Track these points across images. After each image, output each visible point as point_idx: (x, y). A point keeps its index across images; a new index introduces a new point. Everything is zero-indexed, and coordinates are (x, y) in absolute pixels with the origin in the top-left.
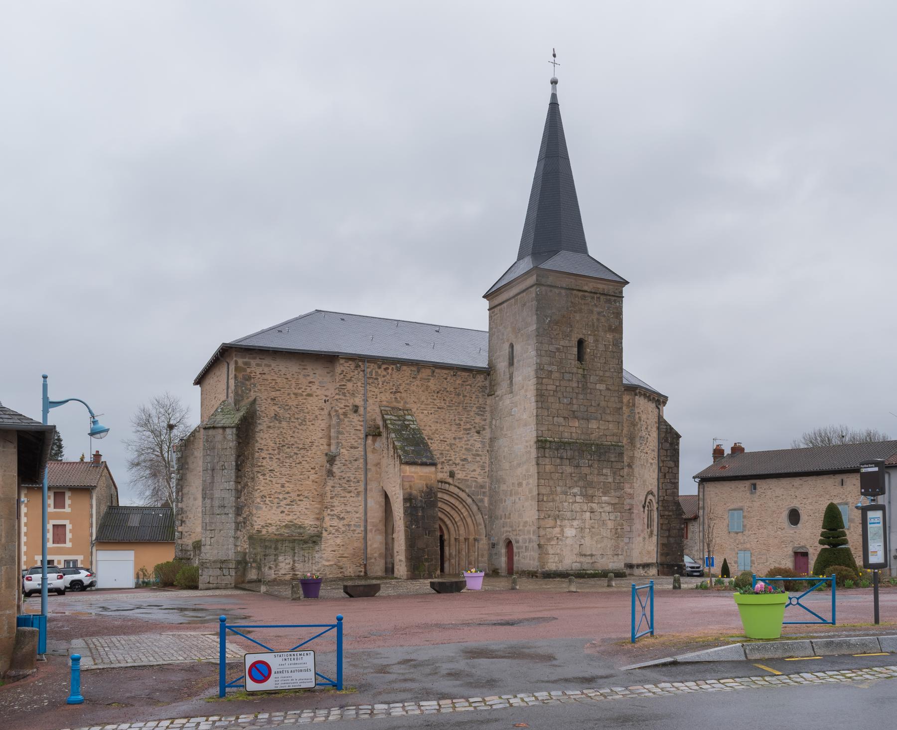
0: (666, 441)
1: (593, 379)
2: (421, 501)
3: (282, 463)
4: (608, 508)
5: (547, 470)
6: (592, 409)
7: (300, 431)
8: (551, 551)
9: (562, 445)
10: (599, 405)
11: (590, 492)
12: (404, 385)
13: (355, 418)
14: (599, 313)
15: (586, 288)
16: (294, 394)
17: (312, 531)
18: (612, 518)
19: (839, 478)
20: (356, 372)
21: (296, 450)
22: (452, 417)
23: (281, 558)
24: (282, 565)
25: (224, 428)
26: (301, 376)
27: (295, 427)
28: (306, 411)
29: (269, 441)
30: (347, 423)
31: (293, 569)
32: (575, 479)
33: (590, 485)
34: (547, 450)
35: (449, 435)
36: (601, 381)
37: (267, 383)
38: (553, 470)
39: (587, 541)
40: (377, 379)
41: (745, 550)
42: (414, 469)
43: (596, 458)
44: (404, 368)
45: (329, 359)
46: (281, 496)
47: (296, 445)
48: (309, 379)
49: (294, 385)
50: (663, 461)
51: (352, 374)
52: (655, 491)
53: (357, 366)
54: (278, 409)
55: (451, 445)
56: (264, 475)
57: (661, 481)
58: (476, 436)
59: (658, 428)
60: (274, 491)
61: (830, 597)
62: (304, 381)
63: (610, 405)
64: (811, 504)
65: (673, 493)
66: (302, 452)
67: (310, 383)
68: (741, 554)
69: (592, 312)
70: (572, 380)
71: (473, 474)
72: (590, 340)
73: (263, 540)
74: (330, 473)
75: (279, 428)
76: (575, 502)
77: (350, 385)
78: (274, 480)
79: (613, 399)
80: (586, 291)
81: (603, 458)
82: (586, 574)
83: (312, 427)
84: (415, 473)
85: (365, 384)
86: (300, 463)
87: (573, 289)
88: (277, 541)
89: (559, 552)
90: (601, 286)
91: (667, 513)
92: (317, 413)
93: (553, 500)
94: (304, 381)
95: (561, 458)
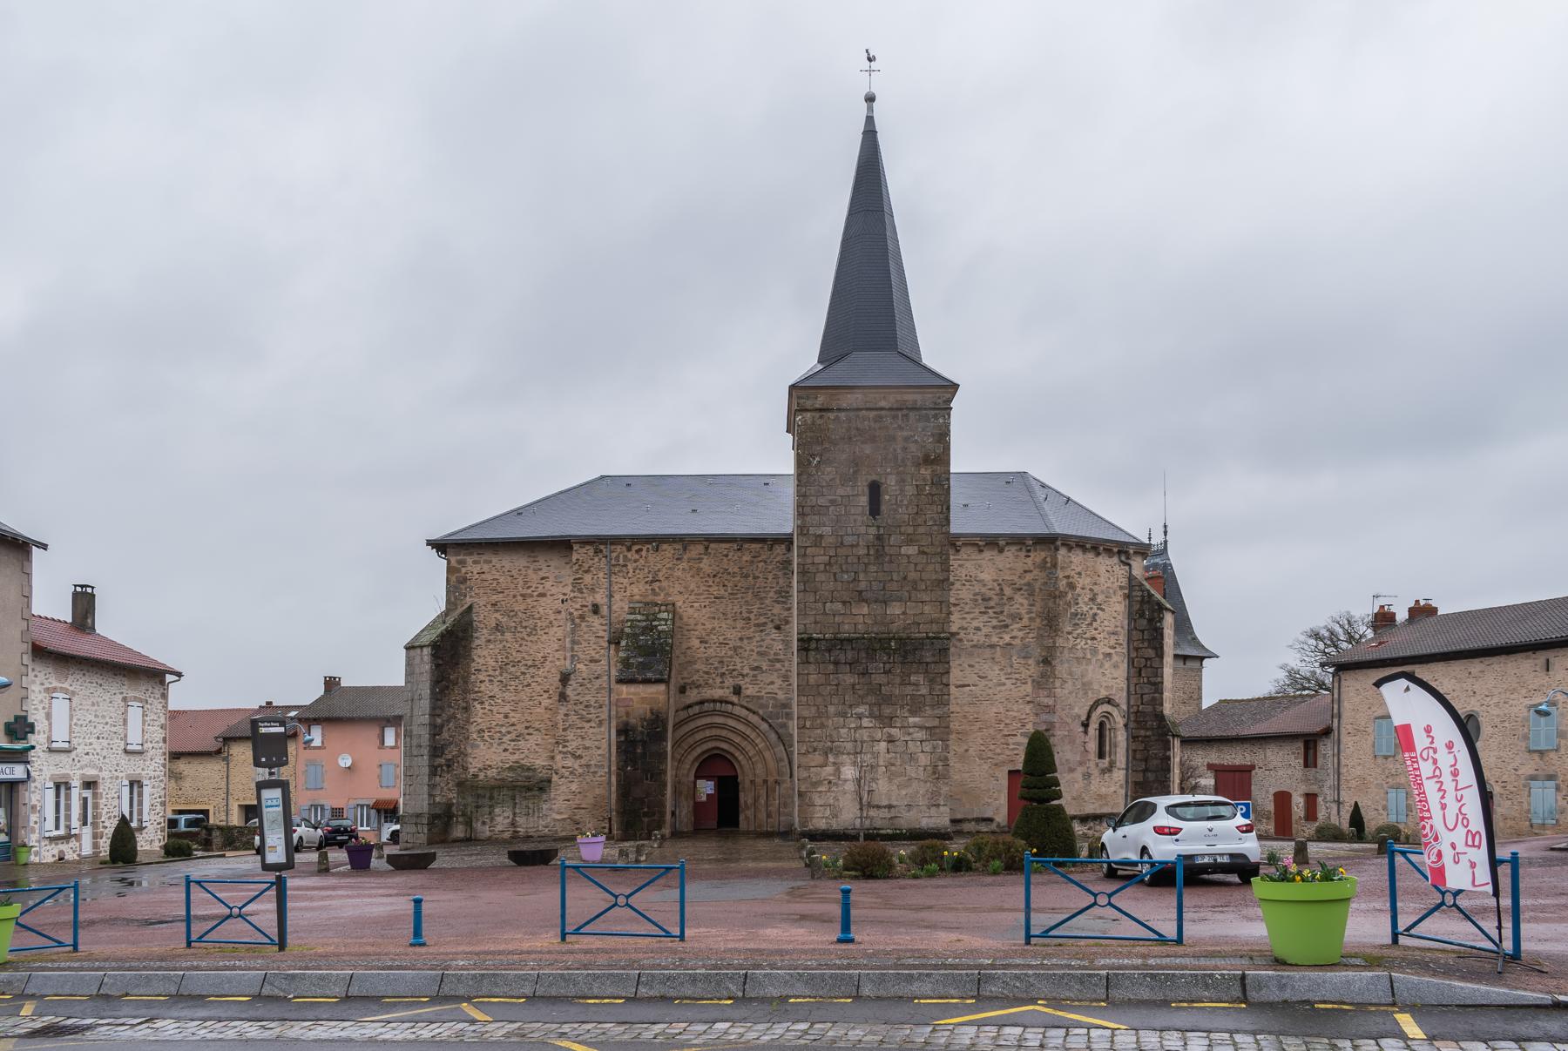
0: (1142, 616)
3: (504, 686)
4: (921, 735)
6: (894, 586)
8: (818, 801)
9: (838, 643)
11: (887, 711)
13: (596, 622)
14: (906, 439)
15: (883, 404)
17: (543, 774)
18: (927, 749)
19: (1541, 657)
21: (523, 669)
22: (737, 609)
23: (497, 810)
24: (499, 819)
25: (421, 647)
26: (530, 572)
31: (513, 824)
33: (889, 700)
35: (733, 635)
36: (910, 541)
38: (822, 681)
41: (1397, 787)
42: (633, 688)
43: (898, 658)
44: (665, 546)
45: (561, 545)
46: (504, 730)
48: (542, 574)
50: (1137, 649)
52: (1121, 698)
53: (598, 551)
55: (735, 649)
57: (1135, 680)
58: (774, 634)
59: (1128, 596)
61: (1022, 889)
62: (534, 577)
63: (924, 576)
64: (1497, 705)
65: (1154, 699)
66: (532, 670)
68: (1392, 794)
69: (892, 439)
71: (770, 688)
72: (891, 482)
73: (474, 788)
74: (563, 697)
76: (861, 727)
77: (588, 578)
78: (495, 709)
79: (931, 567)
81: (910, 658)
88: (493, 788)
91: (1142, 733)
92: (552, 618)
93: (822, 726)
94: (534, 577)
95: (836, 663)
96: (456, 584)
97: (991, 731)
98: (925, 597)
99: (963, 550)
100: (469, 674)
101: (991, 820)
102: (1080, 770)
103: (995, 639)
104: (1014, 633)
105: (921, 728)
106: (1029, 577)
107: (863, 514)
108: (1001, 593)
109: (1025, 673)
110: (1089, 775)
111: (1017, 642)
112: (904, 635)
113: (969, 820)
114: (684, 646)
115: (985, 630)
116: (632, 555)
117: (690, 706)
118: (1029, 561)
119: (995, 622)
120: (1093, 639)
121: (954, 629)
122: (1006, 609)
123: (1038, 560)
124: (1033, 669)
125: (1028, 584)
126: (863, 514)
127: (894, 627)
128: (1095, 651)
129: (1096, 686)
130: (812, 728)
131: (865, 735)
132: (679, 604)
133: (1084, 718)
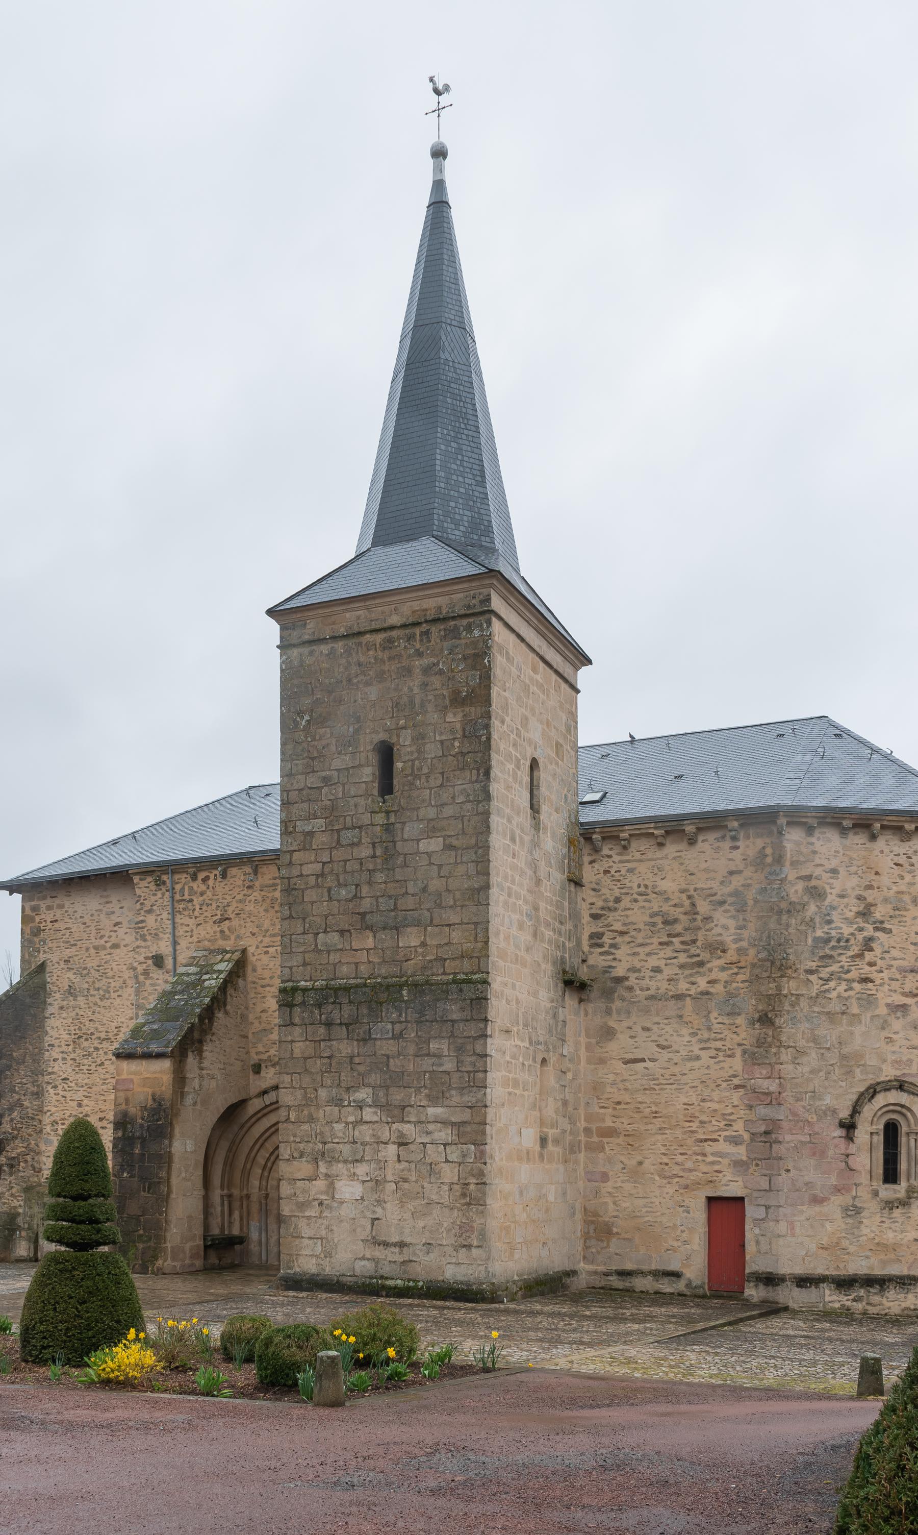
1: (411, 829)
2: (142, 1126)
4: (445, 1134)
5: (297, 1053)
6: (410, 902)
7: (102, 1010)
8: (306, 1232)
9: (332, 993)
10: (424, 890)
11: (397, 1096)
12: (234, 904)
14: (426, 671)
15: (395, 620)
16: (96, 948)
20: (159, 894)
21: (96, 1043)
27: (96, 1004)
28: (110, 974)
29: (61, 1031)
30: (150, 989)
32: (361, 1068)
33: (397, 1080)
34: (297, 1010)
36: (431, 830)
37: (59, 935)
38: (310, 1052)
39: (391, 1212)
40: (191, 901)
43: (412, 1015)
44: (233, 871)
47: (97, 1035)
49: (94, 932)
51: (153, 898)
54: (72, 977)
56: (55, 1087)
60: (68, 1113)
62: (106, 923)
67: (116, 925)
70: (359, 844)
72: (405, 742)
75: (74, 1008)
76: (362, 1122)
77: (151, 920)
78: (68, 1094)
79: (461, 869)
80: (392, 628)
82: (383, 1287)
83: (118, 1001)
84: (135, 1073)
85: (174, 913)
86: (102, 1064)
87: (360, 634)
89: (323, 1233)
90: (431, 604)
93: (311, 1119)
95: (329, 1024)
96: (32, 934)
97: (678, 1133)
98: (454, 918)
99: (634, 844)
100: (41, 1051)
101: (676, 1275)
102: (837, 1201)
103: (683, 986)
104: (713, 976)
105: (445, 1123)
106: (737, 882)
107: (367, 795)
108: (693, 911)
109: (731, 1040)
110: (858, 1210)
111: (718, 988)
112: (420, 979)
113: (642, 1273)
114: (259, 1009)
115: (668, 972)
116: (198, 886)
117: (265, 1092)
118: (737, 855)
119: (683, 958)
120: (865, 980)
121: (620, 972)
122: (700, 935)
123: (752, 853)
124: (744, 1033)
125: (736, 893)
126: (367, 795)
127: (409, 967)
128: (868, 1001)
129: (872, 1061)
130: (299, 1122)
131: (365, 1133)
132: (251, 950)
133: (844, 1114)
